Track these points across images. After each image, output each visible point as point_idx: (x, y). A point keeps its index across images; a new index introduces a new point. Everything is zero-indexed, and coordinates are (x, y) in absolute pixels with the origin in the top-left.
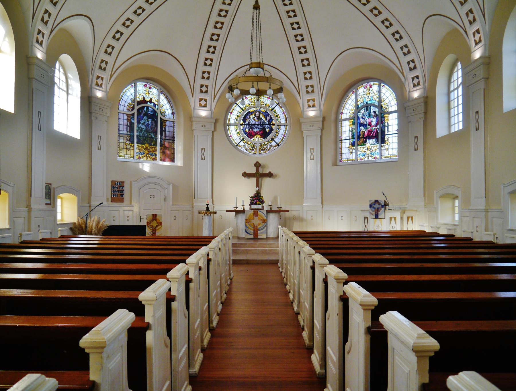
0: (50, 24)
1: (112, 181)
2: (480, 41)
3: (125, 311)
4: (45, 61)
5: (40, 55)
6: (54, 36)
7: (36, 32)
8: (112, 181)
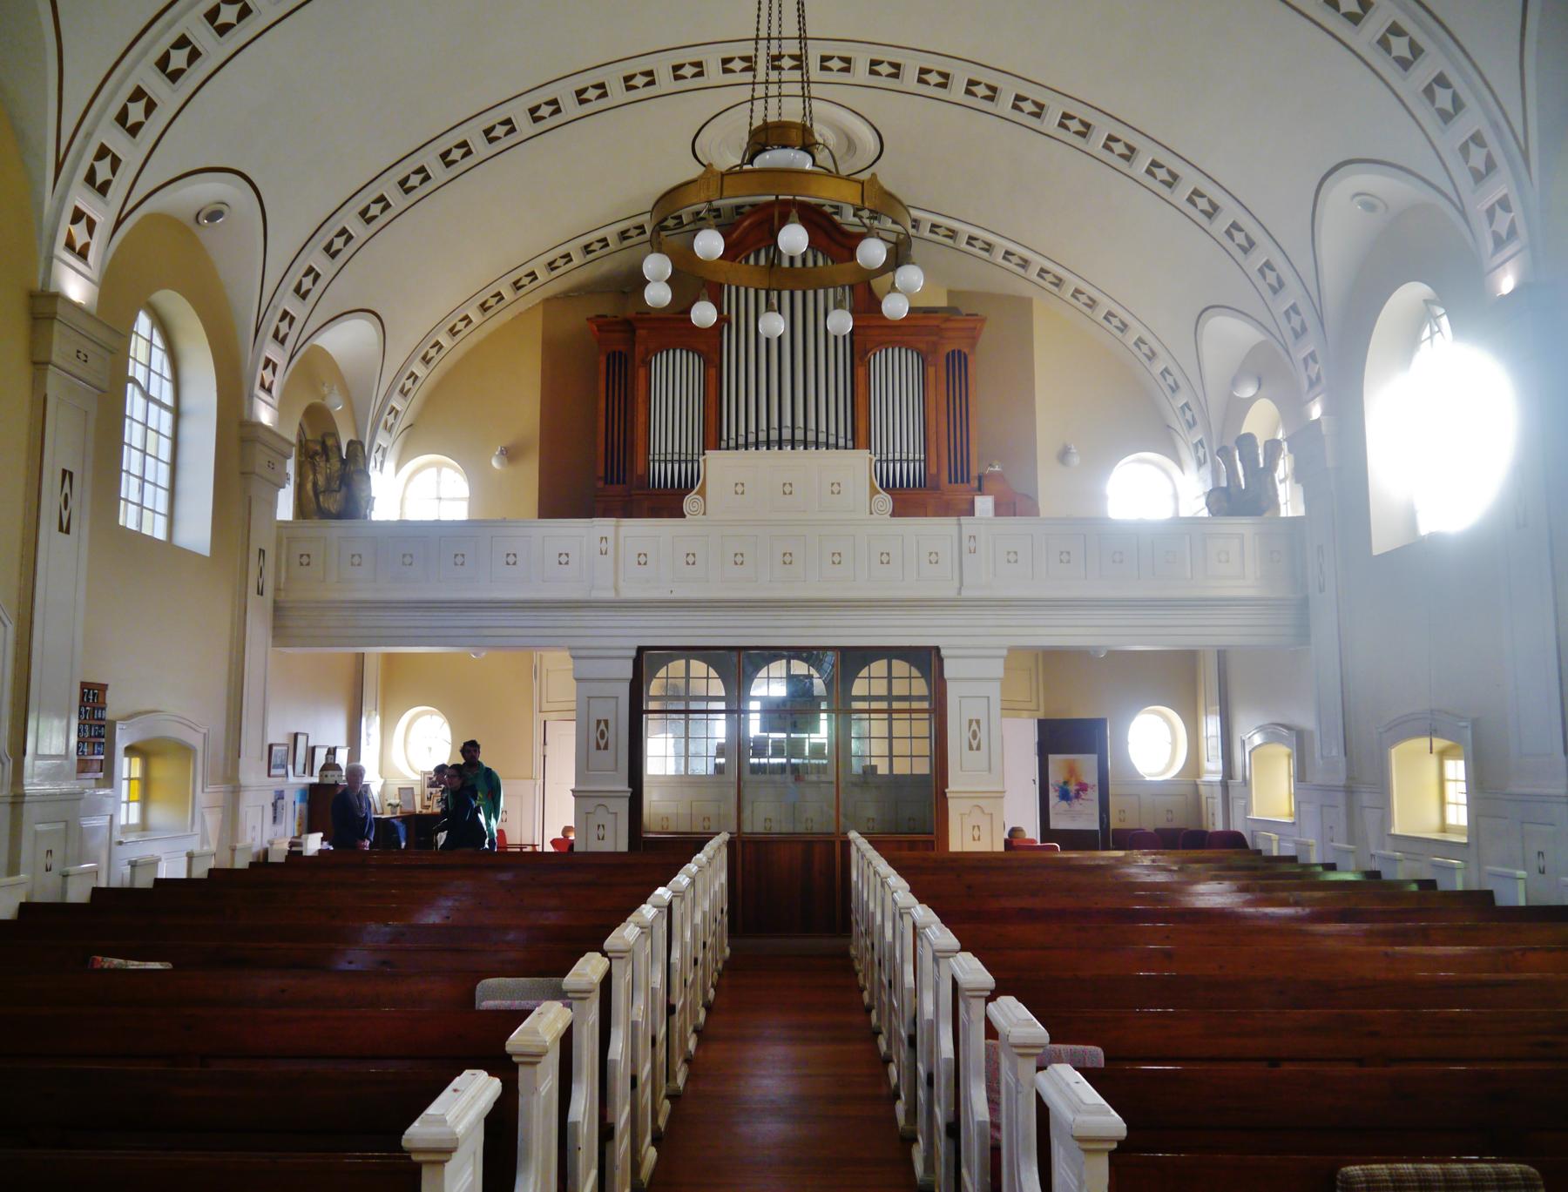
1: (84, 685)
2: (1512, 232)
3: (483, 1075)
4: (94, 311)
5: (76, 287)
7: (68, 214)
8: (84, 685)
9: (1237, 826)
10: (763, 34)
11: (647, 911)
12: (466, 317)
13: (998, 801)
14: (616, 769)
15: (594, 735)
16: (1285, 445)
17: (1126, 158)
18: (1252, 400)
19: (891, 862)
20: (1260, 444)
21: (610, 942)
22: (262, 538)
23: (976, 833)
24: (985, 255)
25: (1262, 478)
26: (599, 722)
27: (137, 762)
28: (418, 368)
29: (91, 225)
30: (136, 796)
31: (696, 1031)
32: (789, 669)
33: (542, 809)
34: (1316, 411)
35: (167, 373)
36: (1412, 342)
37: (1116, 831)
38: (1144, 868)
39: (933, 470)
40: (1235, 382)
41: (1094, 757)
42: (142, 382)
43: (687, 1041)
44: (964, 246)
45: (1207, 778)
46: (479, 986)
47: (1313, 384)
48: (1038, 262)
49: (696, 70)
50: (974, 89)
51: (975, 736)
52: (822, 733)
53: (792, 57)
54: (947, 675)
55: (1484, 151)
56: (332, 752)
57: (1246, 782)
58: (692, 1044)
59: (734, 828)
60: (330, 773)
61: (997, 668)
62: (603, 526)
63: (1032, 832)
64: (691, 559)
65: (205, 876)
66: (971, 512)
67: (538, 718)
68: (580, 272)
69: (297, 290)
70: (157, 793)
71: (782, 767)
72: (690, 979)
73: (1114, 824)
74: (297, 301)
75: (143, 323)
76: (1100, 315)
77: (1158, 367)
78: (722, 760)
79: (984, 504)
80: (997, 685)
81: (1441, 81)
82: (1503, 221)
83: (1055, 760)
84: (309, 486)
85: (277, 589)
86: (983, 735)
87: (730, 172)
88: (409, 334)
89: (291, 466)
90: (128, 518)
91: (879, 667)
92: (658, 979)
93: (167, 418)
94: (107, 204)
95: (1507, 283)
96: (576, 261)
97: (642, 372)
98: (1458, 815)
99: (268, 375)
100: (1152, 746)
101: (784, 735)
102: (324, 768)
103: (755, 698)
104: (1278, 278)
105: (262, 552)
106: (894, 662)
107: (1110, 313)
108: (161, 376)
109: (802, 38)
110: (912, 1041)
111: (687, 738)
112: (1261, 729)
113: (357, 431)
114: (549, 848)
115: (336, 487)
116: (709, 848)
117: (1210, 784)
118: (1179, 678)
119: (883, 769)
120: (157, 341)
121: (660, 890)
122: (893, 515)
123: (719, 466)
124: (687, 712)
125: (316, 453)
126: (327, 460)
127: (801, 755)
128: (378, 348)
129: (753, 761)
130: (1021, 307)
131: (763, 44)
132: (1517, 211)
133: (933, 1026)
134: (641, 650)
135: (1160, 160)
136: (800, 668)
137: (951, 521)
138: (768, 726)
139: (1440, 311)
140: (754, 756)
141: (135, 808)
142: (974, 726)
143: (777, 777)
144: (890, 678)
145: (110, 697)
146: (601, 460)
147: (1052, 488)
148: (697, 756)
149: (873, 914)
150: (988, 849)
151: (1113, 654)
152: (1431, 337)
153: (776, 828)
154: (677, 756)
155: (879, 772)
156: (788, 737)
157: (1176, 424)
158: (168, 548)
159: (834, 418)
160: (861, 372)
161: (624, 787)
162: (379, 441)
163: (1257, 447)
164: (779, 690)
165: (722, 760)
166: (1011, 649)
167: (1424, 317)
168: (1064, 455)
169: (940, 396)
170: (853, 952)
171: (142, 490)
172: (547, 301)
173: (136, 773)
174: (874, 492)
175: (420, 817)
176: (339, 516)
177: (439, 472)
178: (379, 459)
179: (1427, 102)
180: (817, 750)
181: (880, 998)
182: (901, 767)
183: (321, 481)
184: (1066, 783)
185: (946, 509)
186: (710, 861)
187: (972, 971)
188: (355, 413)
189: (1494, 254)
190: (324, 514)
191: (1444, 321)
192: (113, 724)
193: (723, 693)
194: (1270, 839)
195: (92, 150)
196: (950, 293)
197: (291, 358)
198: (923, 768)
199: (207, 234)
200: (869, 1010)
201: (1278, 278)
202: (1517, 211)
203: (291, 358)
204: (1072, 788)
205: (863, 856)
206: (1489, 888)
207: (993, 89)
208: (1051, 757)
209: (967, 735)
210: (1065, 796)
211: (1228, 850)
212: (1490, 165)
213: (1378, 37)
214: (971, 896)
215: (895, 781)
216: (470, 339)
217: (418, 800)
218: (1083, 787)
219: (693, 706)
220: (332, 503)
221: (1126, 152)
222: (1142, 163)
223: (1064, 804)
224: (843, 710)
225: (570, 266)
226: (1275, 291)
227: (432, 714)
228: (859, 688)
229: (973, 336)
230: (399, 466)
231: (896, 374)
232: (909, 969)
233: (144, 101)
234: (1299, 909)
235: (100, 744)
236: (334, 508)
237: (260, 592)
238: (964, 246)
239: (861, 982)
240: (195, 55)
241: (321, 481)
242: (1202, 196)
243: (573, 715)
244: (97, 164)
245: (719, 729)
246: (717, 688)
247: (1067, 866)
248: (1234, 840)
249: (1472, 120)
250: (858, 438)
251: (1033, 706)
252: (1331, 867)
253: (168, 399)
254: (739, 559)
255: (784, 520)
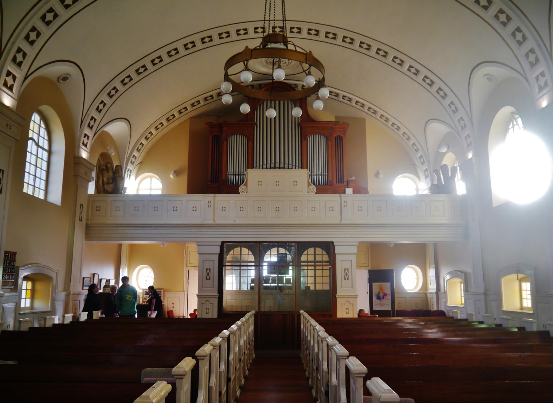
0: (94, 128)
1: (6, 252)
4: (15, 110)
6: (31, 82)
8: (6, 252)
9: (442, 308)
10: (267, 18)
11: (218, 340)
12: (161, 123)
13: (354, 299)
14: (213, 287)
15: (205, 274)
16: (458, 168)
17: (400, 65)
18: (445, 154)
19: (317, 321)
20: (449, 168)
21: (199, 353)
22: (82, 200)
23: (347, 311)
24: (348, 102)
25: (450, 180)
26: (207, 269)
27: (30, 283)
28: (144, 141)
29: (14, 78)
30: (29, 296)
31: (240, 388)
32: (278, 251)
33: (186, 303)
34: (470, 156)
35: (46, 137)
36: (505, 130)
37: (397, 311)
38: (408, 323)
39: (330, 179)
40: (439, 147)
41: (389, 284)
42: (36, 140)
43: (236, 392)
44: (341, 99)
45: (430, 291)
46: (143, 372)
47: (468, 146)
48: (368, 105)
49: (245, 32)
50: (345, 39)
51: (346, 275)
52: (290, 275)
53: (280, 27)
54: (336, 252)
55: (534, 55)
56: (108, 281)
57: (445, 292)
58: (238, 393)
59: (257, 310)
60: (107, 289)
61: (355, 250)
62: (210, 197)
63: (367, 311)
64: (242, 209)
65: (51, 326)
66: (344, 192)
67: (186, 269)
68: (203, 108)
69: (97, 109)
70: (37, 295)
71: (275, 288)
72: (238, 367)
73: (397, 308)
74: (97, 113)
75: (36, 117)
76: (390, 124)
77: (411, 143)
78: (253, 285)
79: (349, 191)
80: (355, 256)
81: (518, 30)
82: (542, 81)
83: (375, 285)
84: (101, 182)
85: (87, 220)
86: (349, 274)
87: (255, 49)
88: (141, 127)
89: (94, 174)
90: (28, 189)
91: (311, 250)
92: (223, 367)
93: (45, 154)
94: (21, 70)
95: (544, 103)
96: (202, 104)
97: (225, 142)
98: (528, 303)
99: (85, 140)
100: (410, 280)
101: (276, 275)
102: (105, 287)
103: (265, 262)
104: (456, 107)
105: (82, 205)
106: (317, 249)
107: (393, 123)
108: (44, 138)
109: (284, 20)
110: (327, 393)
111: (240, 276)
112: (449, 273)
113: (120, 162)
114: (189, 317)
115: (111, 182)
116: (247, 316)
117: (432, 293)
118: (418, 254)
119: (312, 288)
120: (42, 125)
121: (225, 331)
122: (316, 193)
123: (253, 175)
124: (241, 266)
125: (103, 169)
126: (108, 172)
127: (282, 283)
128: (128, 133)
129: (264, 285)
130: (362, 122)
131: (267, 22)
132: (548, 77)
133: (337, 388)
134: (223, 243)
135: (413, 65)
136: (282, 250)
137: (337, 196)
138: (270, 272)
139: (517, 116)
140: (265, 283)
141: (28, 301)
142: (346, 271)
143: (274, 291)
144: (315, 254)
145: (17, 257)
146: (209, 175)
147: (372, 185)
148: (244, 283)
149: (310, 341)
150: (352, 317)
151: (396, 245)
152: (513, 127)
153: (273, 310)
154: (237, 283)
155: (311, 289)
156: (278, 276)
157: (418, 164)
158: (45, 203)
159: (294, 156)
160: (304, 143)
161: (216, 294)
162: (129, 167)
163: (448, 169)
164: (274, 259)
165: (253, 285)
166: (360, 243)
167: (511, 119)
168: (377, 175)
169: (332, 147)
170: (302, 356)
171: (35, 180)
172: (191, 118)
173: (29, 287)
174: (309, 185)
175: (142, 305)
176: (112, 192)
177: (151, 180)
178: (129, 174)
179: (513, 38)
180: (288, 281)
181: (312, 374)
182: (319, 287)
183: (105, 179)
184: (379, 293)
185: (335, 192)
186: (247, 321)
187: (356, 364)
188: (120, 156)
189: (538, 93)
190: (106, 192)
191: (519, 120)
192: (18, 268)
193: (254, 260)
194: (457, 312)
195: (15, 49)
196: (336, 117)
197: (95, 134)
198: (327, 287)
199: (64, 87)
200: (308, 379)
201: (456, 107)
202: (548, 77)
203: (95, 134)
204: (381, 295)
205: (306, 319)
206: (548, 330)
207: (352, 39)
208: (374, 284)
209: (344, 274)
210: (379, 298)
211: (440, 317)
212: (537, 60)
213: (494, 14)
214: (350, 333)
215: (316, 292)
216: (163, 131)
217: (141, 299)
218: (385, 295)
219: (243, 264)
220: (109, 188)
221: (400, 62)
222: (406, 66)
223: (378, 301)
224: (297, 265)
225: (199, 105)
226: (454, 112)
227: (147, 268)
228: (304, 258)
229: (345, 131)
230: (136, 178)
231: (317, 145)
232: (325, 363)
233: (36, 32)
234: (470, 338)
235: (12, 275)
236: (110, 190)
237: (81, 220)
238: (341, 99)
239: (305, 367)
240: (56, 16)
241: (105, 179)
242: (428, 78)
243: (197, 268)
244: (17, 55)
245: (252, 273)
246: (252, 258)
247: (379, 323)
248: (441, 313)
249: (530, 43)
250: (303, 165)
251: (366, 265)
252: (482, 323)
253: (46, 147)
254: (259, 209)
255: (277, 196)
